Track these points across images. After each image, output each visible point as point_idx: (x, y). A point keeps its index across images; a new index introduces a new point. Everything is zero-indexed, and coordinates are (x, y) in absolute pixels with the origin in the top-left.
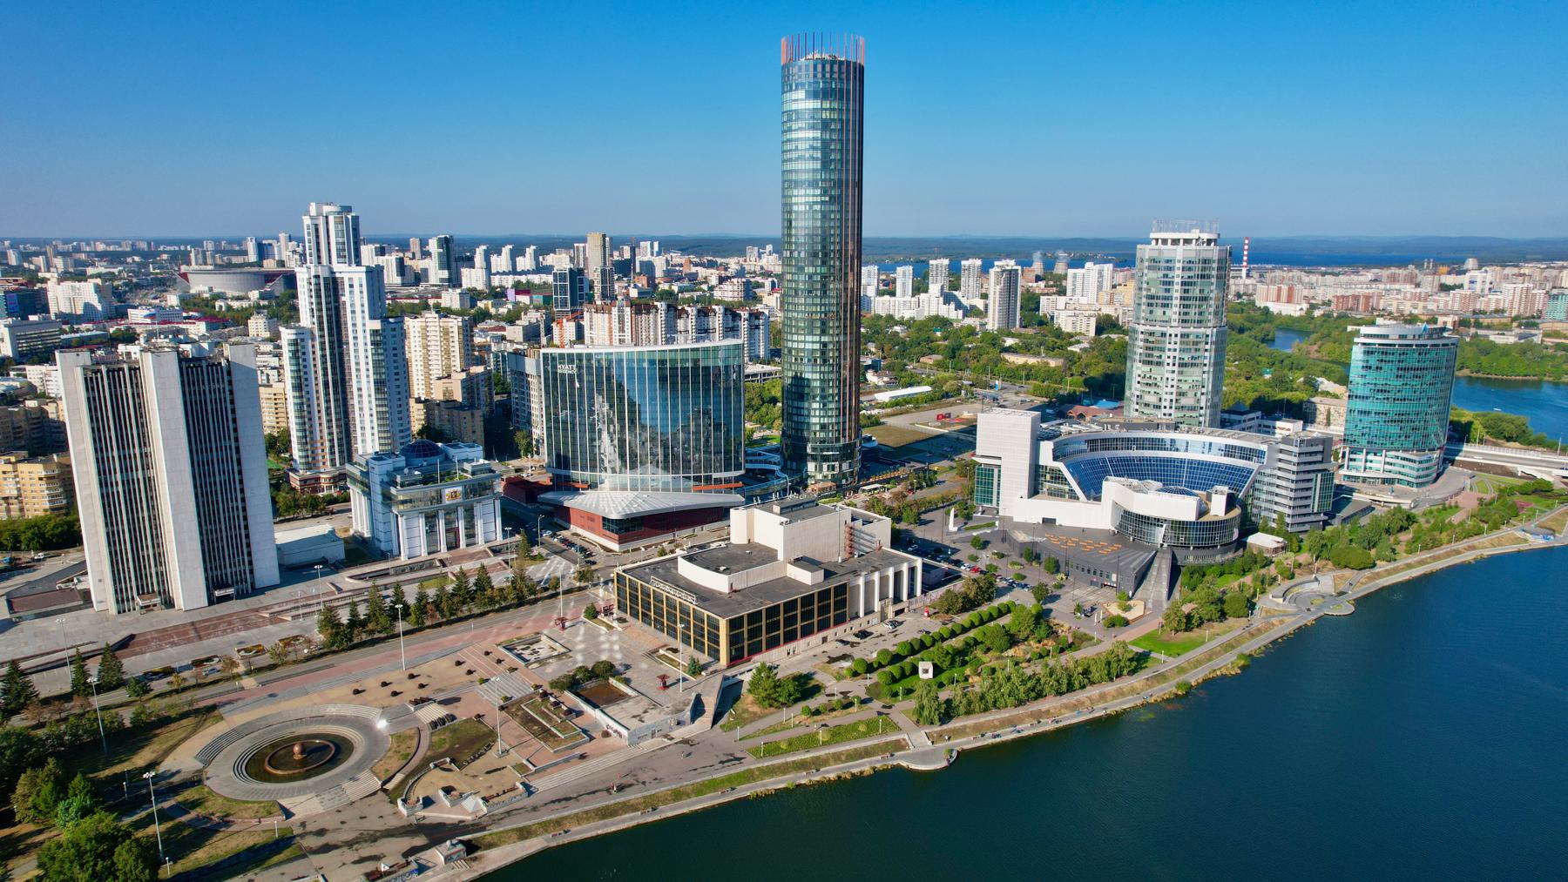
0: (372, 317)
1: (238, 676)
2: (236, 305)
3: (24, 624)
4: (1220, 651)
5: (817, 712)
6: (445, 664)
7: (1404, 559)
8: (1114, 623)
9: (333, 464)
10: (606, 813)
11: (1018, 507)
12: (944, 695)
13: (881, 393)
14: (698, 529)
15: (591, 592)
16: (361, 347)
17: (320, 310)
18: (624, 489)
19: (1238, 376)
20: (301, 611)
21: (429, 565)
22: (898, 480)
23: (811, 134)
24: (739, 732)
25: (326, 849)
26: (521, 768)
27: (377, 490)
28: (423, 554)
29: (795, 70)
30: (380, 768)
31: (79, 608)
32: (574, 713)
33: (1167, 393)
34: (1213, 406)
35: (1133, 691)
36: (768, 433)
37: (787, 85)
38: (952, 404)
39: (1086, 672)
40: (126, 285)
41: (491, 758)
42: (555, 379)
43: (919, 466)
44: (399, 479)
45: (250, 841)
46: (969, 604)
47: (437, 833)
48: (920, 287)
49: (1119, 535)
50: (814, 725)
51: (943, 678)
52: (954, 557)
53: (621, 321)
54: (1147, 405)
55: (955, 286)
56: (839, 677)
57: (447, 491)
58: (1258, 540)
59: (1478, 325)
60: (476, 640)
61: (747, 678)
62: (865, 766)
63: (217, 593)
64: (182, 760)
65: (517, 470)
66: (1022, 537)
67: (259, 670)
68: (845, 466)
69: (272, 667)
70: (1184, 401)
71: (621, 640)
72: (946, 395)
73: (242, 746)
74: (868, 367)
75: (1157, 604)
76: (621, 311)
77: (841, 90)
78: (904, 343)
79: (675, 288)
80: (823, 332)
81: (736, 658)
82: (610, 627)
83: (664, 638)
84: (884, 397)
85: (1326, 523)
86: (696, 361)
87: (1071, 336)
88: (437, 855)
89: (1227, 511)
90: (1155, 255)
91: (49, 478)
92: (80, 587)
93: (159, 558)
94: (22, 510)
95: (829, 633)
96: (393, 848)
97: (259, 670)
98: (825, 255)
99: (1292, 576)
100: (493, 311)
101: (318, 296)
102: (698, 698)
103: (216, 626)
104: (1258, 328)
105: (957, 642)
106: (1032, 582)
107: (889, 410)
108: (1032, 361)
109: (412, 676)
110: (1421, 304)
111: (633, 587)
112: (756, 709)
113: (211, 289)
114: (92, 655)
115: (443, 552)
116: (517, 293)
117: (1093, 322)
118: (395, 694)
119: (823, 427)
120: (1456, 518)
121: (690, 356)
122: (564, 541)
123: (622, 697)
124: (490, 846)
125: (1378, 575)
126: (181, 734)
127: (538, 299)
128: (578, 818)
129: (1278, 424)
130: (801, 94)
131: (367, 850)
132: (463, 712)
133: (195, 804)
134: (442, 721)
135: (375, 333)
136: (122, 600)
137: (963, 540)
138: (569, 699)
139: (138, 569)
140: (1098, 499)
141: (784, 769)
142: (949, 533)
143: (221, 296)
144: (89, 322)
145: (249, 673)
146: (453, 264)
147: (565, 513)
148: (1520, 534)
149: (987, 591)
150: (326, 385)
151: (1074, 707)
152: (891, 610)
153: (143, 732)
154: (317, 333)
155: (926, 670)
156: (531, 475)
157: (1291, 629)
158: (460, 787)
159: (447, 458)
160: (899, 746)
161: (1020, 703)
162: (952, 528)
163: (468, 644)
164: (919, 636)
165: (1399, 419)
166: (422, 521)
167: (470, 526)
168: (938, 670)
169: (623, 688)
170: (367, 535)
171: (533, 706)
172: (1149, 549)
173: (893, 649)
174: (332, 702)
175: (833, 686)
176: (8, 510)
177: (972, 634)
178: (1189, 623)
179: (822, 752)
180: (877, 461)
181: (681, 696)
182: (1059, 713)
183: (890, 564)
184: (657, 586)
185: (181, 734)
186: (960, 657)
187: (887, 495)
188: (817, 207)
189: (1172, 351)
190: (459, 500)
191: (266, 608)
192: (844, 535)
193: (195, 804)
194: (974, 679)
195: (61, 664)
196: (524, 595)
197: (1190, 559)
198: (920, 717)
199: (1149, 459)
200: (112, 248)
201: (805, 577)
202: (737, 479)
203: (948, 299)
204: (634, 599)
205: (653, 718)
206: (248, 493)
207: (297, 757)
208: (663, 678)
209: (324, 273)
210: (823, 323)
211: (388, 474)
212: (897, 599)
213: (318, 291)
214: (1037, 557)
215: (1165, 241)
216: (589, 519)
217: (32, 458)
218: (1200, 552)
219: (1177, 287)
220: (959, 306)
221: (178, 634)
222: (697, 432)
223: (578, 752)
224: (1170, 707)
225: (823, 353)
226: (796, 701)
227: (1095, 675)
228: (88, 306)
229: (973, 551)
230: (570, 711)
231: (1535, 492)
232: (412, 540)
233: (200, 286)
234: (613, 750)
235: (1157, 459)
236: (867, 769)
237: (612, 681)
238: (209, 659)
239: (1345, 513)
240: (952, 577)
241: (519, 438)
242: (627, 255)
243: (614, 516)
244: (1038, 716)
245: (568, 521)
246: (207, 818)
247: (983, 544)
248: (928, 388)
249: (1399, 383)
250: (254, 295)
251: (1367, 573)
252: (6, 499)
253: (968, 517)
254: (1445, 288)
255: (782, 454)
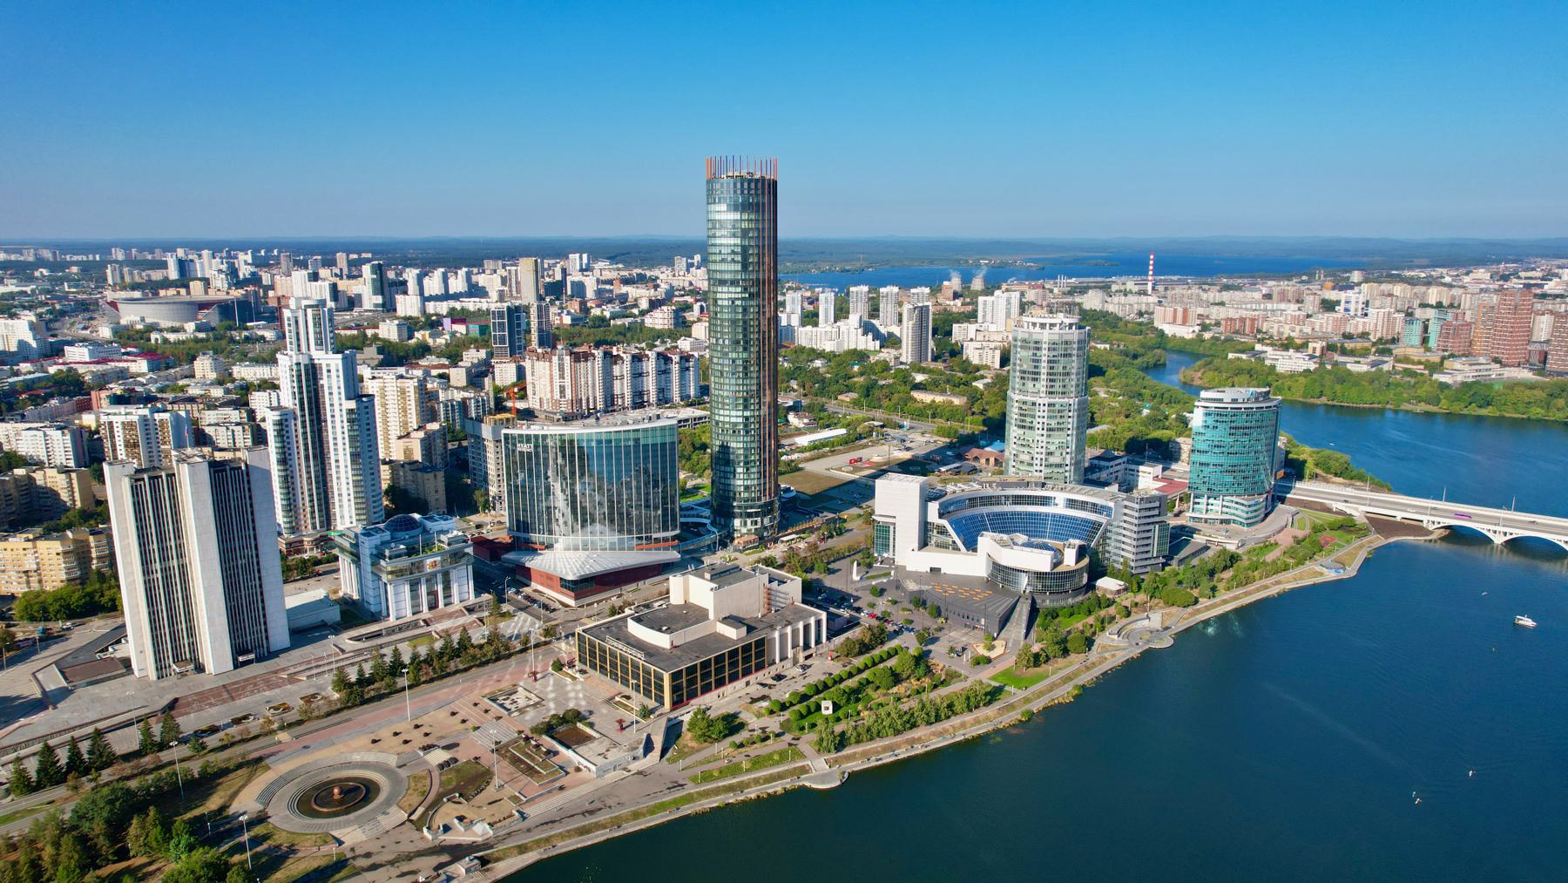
0: (348, 398)
1: (273, 732)
2: (172, 337)
3: (79, 691)
4: (1062, 681)
5: (741, 745)
6: (443, 715)
7: (1223, 595)
8: (981, 661)
9: (314, 527)
10: (583, 831)
11: (909, 557)
12: (838, 728)
13: (802, 437)
14: (641, 583)
15: (555, 645)
16: (338, 424)
17: (301, 393)
18: (576, 549)
19: (1118, 414)
20: (314, 671)
21: (415, 625)
22: (812, 530)
23: (732, 241)
24: (681, 764)
25: (374, 867)
26: (515, 799)
27: (366, 560)
28: (409, 616)
29: (718, 186)
30: (405, 803)
31: (122, 675)
32: (552, 753)
33: (1038, 453)
34: (1077, 464)
35: (987, 719)
36: (699, 481)
37: (711, 198)
38: (865, 446)
39: (950, 706)
40: (51, 312)
41: (490, 791)
43: (831, 515)
44: (387, 553)
45: (315, 864)
46: (865, 648)
47: (458, 852)
48: (841, 312)
49: (990, 583)
50: (740, 757)
51: (840, 713)
52: (856, 605)
53: (561, 369)
55: (874, 312)
56: (759, 715)
57: (429, 561)
58: (1107, 584)
59: (1344, 352)
60: (464, 694)
61: (687, 718)
62: (777, 787)
63: (241, 659)
64: (246, 803)
65: (479, 526)
66: (912, 586)
67: (290, 725)
68: (766, 521)
69: (300, 723)
70: (1052, 460)
71: (584, 689)
72: (860, 437)
73: (291, 790)
74: (790, 409)
75: (1016, 642)
76: (561, 359)
77: (758, 204)
78: (823, 380)
79: (607, 314)
80: (746, 408)
81: (677, 703)
82: (574, 678)
83: (619, 686)
84: (803, 441)
85: (1165, 565)
86: (637, 440)
87: (977, 369)
88: (459, 868)
89: (1077, 562)
91: (65, 553)
92: (118, 655)
93: (191, 631)
94: (40, 582)
95: (751, 678)
96: (426, 864)
97: (290, 725)
98: (746, 342)
99: (1128, 614)
100: (430, 341)
101: (300, 381)
102: (649, 737)
103: (244, 688)
104: (1150, 354)
105: (851, 683)
106: (918, 627)
107: (807, 454)
108: (939, 399)
109: (417, 727)
110: (1298, 328)
111: (592, 645)
112: (694, 744)
113: (143, 320)
114: (153, 715)
115: (426, 613)
116: (453, 322)
117: (998, 353)
118: (406, 742)
119: (747, 488)
120: (1270, 557)
121: (632, 436)
122: (527, 598)
123: (589, 738)
124: (498, 860)
125: (1199, 611)
126: (238, 782)
127: (475, 330)
128: (562, 836)
129: (1141, 468)
130: (724, 207)
131: (405, 867)
132: (463, 755)
133: (266, 838)
134: (447, 763)
135: (350, 411)
136: (161, 668)
137: (863, 589)
138: (547, 742)
139: (174, 639)
140: (975, 550)
141: (717, 792)
142: (853, 582)
143: (153, 328)
144: (26, 360)
145: (282, 728)
146: (386, 289)
147: (527, 573)
148: (1319, 568)
149: (880, 637)
150: (307, 458)
151: (940, 734)
152: (801, 656)
153: (207, 783)
154: (298, 413)
155: (827, 708)
156: (490, 533)
157: (1119, 662)
158: (469, 815)
159: (425, 531)
160: (804, 770)
161: (898, 732)
162: (856, 577)
163: (459, 696)
164: (823, 678)
165: (1232, 470)
166: (407, 587)
167: (447, 588)
168: (836, 707)
169: (588, 730)
170: (356, 597)
171: (518, 748)
172: (1011, 594)
173: (802, 690)
174: (356, 750)
175: (754, 722)
176: (28, 583)
177: (864, 675)
178: (1037, 660)
179: (745, 778)
180: (795, 509)
181: (635, 735)
182: (929, 739)
183: (801, 618)
184: (611, 644)
185: (238, 782)
186: (855, 695)
187: (802, 545)
188: (738, 303)
189: (1041, 418)
190: (438, 568)
191: (284, 670)
192: (762, 599)
193: (266, 838)
194: (865, 714)
195: (129, 724)
196: (499, 651)
197: (1046, 603)
198: (821, 747)
199: (1020, 514)
200: (13, 257)
201: (731, 633)
202: (674, 538)
203: (867, 328)
204: (593, 654)
205: (614, 755)
206: (263, 574)
207: (337, 797)
208: (620, 722)
209: (304, 360)
210: (745, 400)
211: (376, 547)
212: (807, 646)
213: (299, 376)
214: (924, 603)
215: (1034, 324)
216: (548, 579)
217: (46, 535)
218: (1055, 597)
219: (1044, 364)
220: (877, 336)
221: (214, 696)
222: (638, 488)
223: (557, 784)
224: (1014, 731)
225: (746, 426)
226: (725, 736)
227: (958, 708)
228: (22, 344)
229: (871, 598)
230: (549, 752)
231: (1341, 527)
232: (399, 603)
233: (131, 316)
234: (583, 782)
235: (1026, 514)
236: (779, 790)
237: (579, 725)
238: (245, 717)
239: (1182, 554)
240: (852, 623)
241: (478, 496)
242: (558, 277)
243: (571, 577)
244: (912, 742)
245: (529, 577)
246: (278, 847)
247: (880, 592)
248: (843, 431)
249: (1231, 439)
250: (190, 326)
251: (1189, 610)
252: (26, 572)
253: (870, 566)
254: (1329, 306)
255: (711, 507)
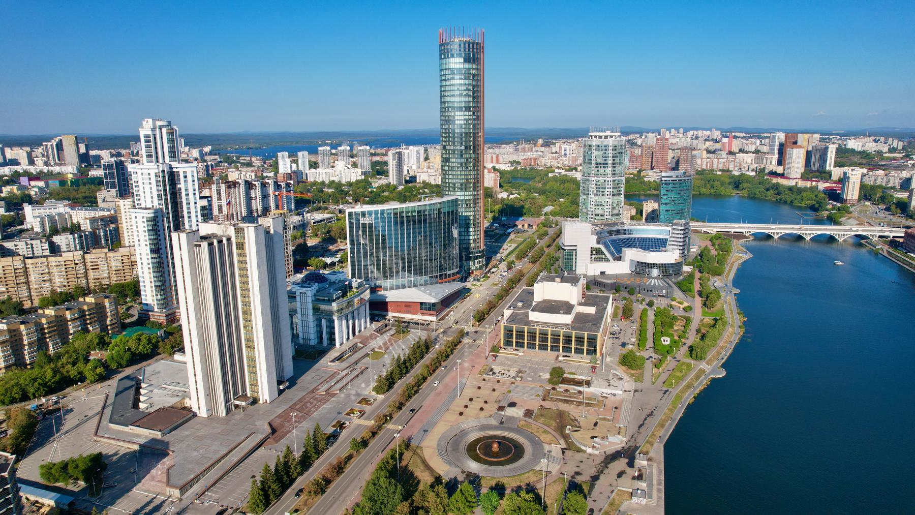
42: (358, 228)
54: (597, 215)
90: (599, 143)
121: (428, 208)
188: (470, 122)
213: (164, 181)
